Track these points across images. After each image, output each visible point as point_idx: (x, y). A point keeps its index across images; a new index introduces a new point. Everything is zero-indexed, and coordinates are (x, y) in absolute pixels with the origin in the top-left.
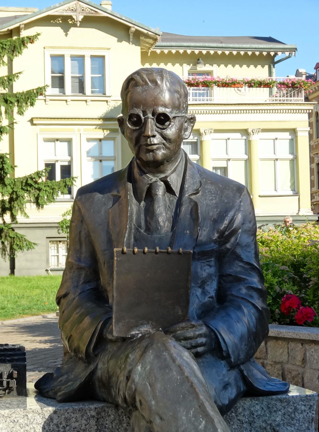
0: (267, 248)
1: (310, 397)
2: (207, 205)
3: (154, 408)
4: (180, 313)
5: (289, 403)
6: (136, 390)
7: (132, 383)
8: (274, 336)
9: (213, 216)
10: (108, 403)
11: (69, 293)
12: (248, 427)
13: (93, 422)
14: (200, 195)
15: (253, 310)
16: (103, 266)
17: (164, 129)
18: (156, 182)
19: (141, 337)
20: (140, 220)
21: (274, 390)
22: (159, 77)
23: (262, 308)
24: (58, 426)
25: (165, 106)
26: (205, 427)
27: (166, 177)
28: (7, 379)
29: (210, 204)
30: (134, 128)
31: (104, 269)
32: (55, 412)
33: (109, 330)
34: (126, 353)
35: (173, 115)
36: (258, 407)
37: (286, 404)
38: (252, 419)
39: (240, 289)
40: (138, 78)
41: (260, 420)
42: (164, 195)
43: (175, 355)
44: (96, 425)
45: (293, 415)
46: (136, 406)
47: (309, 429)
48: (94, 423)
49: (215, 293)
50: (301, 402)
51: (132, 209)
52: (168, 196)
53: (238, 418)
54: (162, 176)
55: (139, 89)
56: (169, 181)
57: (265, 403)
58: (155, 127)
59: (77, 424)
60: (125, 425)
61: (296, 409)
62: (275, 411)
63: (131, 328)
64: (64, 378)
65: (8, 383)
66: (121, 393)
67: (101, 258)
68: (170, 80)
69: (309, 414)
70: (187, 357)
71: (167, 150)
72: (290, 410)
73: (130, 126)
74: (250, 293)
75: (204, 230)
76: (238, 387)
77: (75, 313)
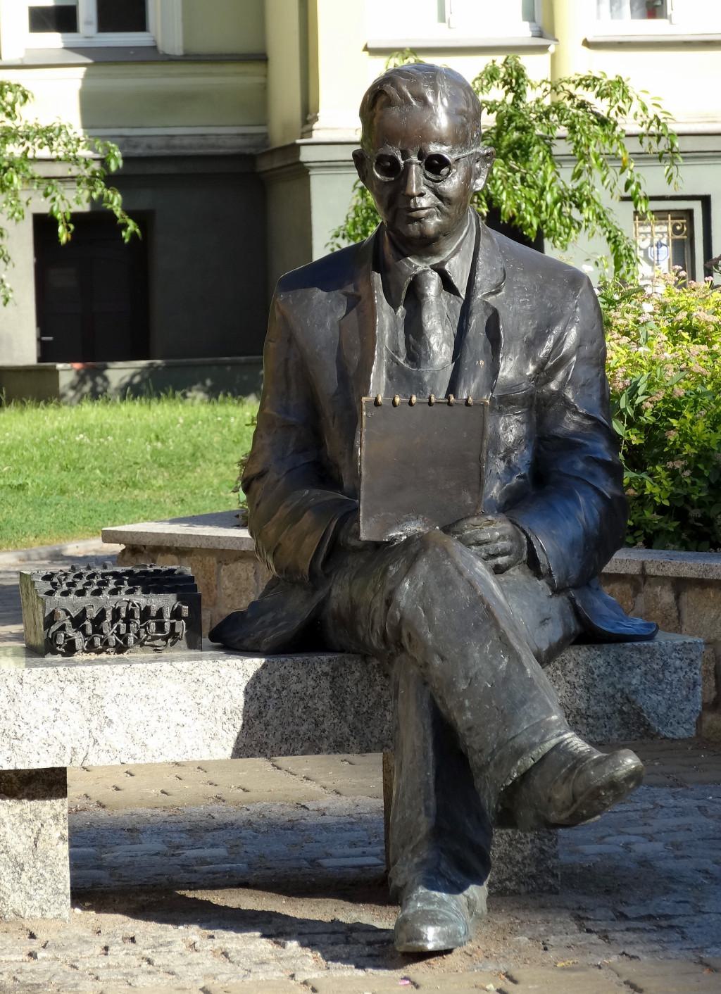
0: (705, 348)
1: (691, 646)
2: (516, 313)
3: (430, 643)
4: (469, 502)
5: (654, 654)
6: (402, 618)
7: (395, 609)
8: (696, 577)
9: (525, 334)
10: (349, 653)
11: (267, 471)
12: (583, 695)
13: (325, 683)
14: (502, 295)
15: (595, 500)
16: (331, 422)
17: (439, 181)
18: (424, 271)
19: (406, 540)
20: (397, 341)
21: (628, 634)
22: (430, 90)
23: (613, 496)
24: (268, 690)
25: (442, 142)
26: (508, 666)
27: (443, 263)
28: (171, 619)
29: (522, 311)
30: (386, 179)
31: (332, 430)
32: (264, 666)
33: (352, 531)
34: (384, 566)
35: (455, 156)
36: (600, 661)
37: (648, 656)
38: (591, 681)
39: (573, 462)
40: (392, 91)
41: (605, 683)
42: (438, 296)
43: (462, 565)
44: (331, 688)
45: (661, 676)
46: (402, 645)
47: (689, 700)
48: (328, 685)
49: (529, 469)
50: (674, 654)
51: (382, 321)
52: (445, 297)
53: (568, 679)
54: (436, 260)
55: (395, 112)
56: (447, 270)
57: (611, 655)
58: (422, 178)
59: (299, 687)
60: (378, 688)
61: (665, 665)
62: (629, 668)
63: (390, 527)
64: (269, 617)
65: (173, 626)
66: (377, 628)
67: (328, 409)
68: (449, 93)
69: (689, 673)
70: (481, 570)
71: (444, 217)
72: (655, 666)
73: (378, 175)
74: (590, 469)
75: (511, 360)
76: (566, 625)
77: (282, 507)
